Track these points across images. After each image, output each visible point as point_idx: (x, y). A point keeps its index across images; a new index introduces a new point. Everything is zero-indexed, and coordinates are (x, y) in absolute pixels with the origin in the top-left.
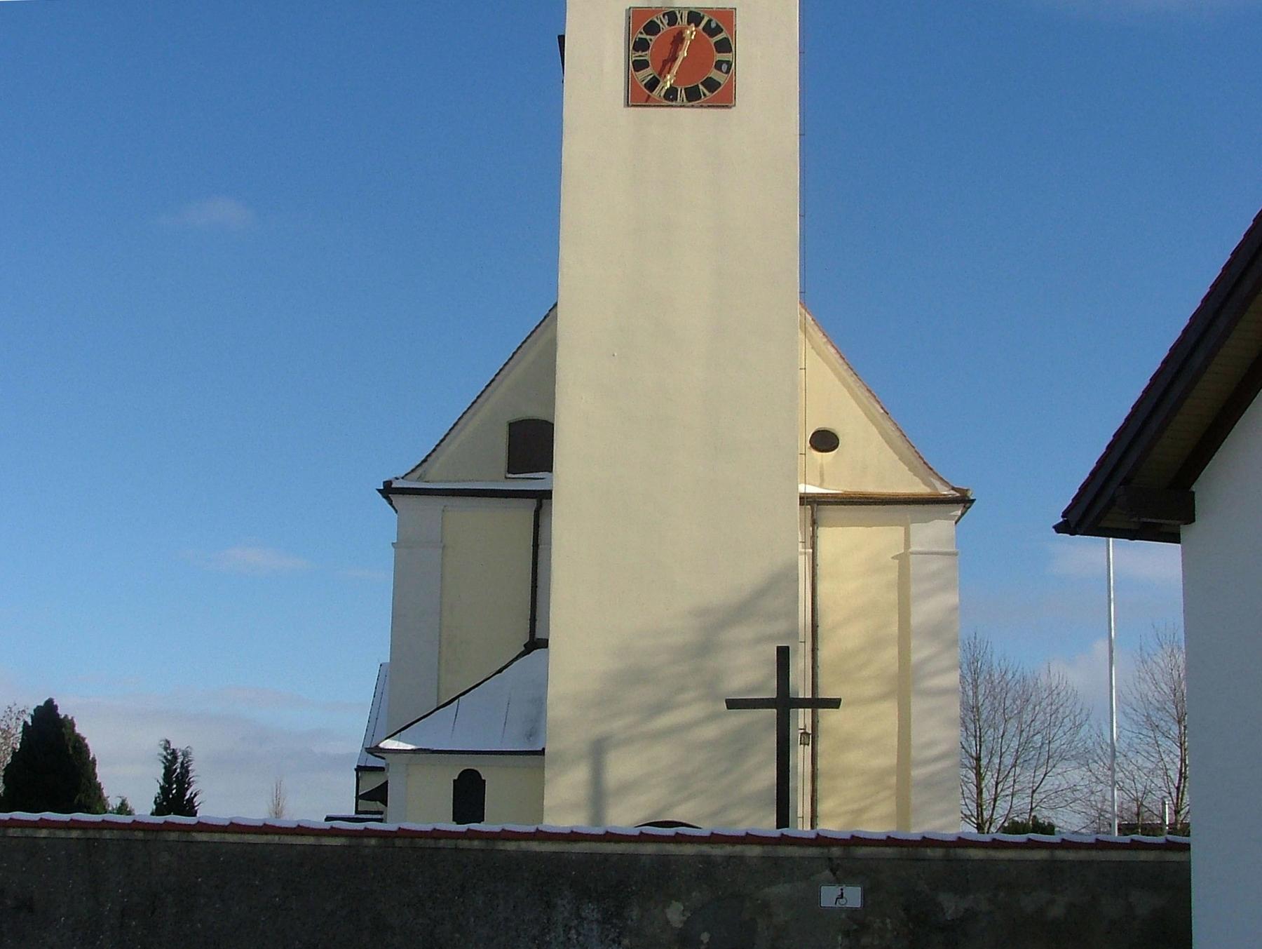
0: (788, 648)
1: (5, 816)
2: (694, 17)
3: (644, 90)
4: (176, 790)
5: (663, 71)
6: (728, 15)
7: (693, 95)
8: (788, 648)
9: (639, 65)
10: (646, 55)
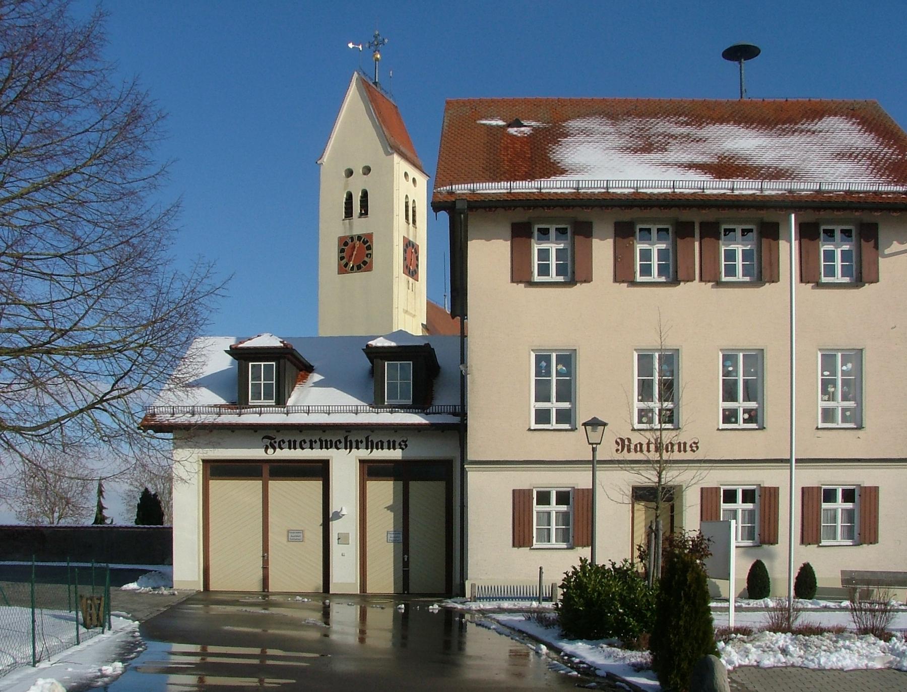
0: (876, 489)
1: (2, 563)
2: (359, 238)
3: (343, 269)
4: (613, 564)
5: (350, 261)
6: (370, 236)
7: (359, 268)
8: (876, 489)
9: (342, 258)
10: (344, 254)
